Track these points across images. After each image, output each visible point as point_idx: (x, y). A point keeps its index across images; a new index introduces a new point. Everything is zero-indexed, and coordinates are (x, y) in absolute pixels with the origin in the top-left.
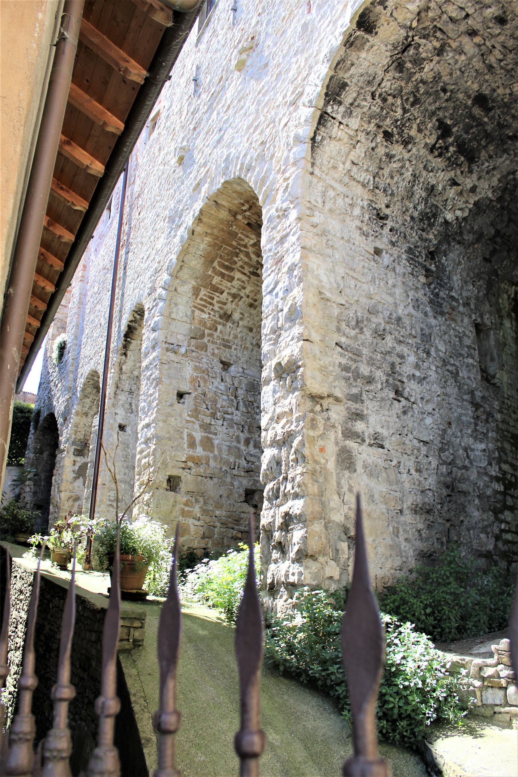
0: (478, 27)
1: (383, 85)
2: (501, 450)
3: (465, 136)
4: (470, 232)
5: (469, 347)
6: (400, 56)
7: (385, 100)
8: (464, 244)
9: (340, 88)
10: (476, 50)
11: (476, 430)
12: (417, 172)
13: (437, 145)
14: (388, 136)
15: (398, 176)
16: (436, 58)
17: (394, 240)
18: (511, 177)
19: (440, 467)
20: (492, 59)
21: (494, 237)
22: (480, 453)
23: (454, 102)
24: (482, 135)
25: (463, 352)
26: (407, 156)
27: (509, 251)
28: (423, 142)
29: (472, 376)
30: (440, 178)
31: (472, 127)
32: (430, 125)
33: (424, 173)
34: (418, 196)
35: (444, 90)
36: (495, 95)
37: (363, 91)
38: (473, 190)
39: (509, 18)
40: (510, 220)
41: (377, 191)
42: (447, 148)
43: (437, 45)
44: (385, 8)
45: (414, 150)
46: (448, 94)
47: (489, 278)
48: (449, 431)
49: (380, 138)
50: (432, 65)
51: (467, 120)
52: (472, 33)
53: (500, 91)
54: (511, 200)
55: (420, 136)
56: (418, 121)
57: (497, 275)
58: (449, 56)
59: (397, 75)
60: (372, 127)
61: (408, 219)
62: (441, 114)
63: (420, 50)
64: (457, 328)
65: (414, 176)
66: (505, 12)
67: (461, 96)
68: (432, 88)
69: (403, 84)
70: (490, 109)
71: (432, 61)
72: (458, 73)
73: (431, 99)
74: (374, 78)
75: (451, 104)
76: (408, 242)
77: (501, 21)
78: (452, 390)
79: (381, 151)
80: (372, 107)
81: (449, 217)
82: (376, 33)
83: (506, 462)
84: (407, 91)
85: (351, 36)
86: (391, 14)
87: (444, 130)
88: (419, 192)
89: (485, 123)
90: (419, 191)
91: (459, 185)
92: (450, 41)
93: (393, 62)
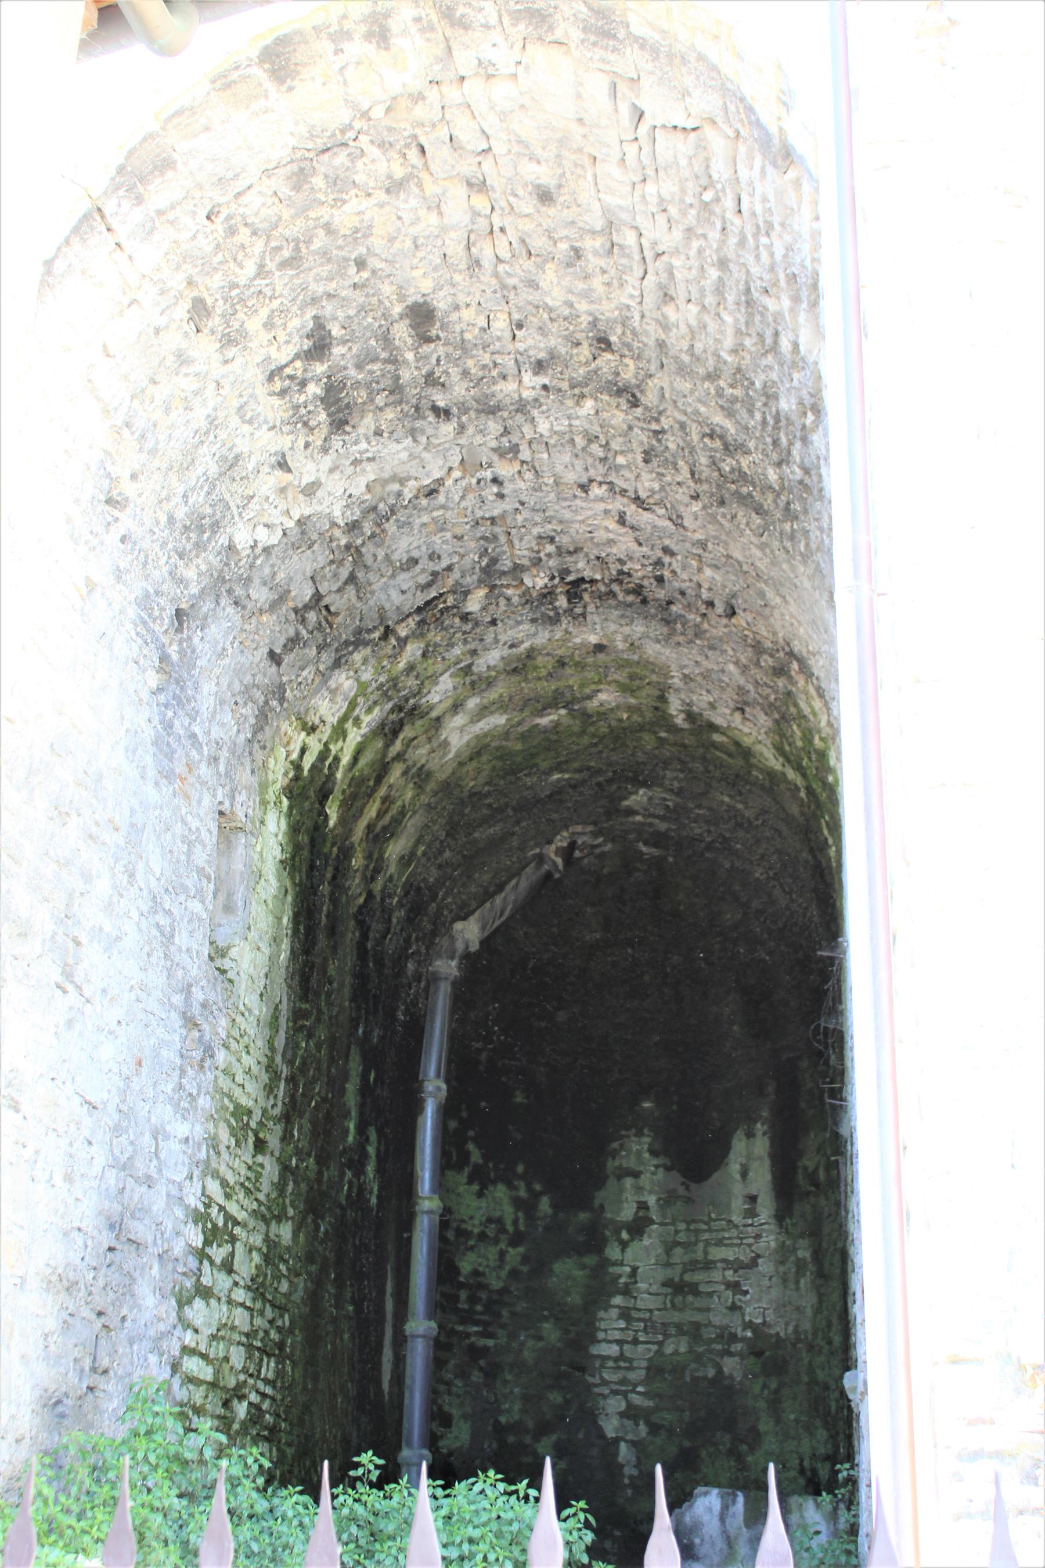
0: (496, 184)
1: (244, 199)
2: (213, 1143)
3: (352, 372)
4: (265, 584)
5: (201, 871)
6: (311, 155)
7: (232, 231)
8: (244, 607)
9: (155, 167)
10: (467, 219)
11: (180, 1087)
12: (221, 415)
13: (288, 371)
14: (200, 309)
15: (181, 410)
16: (382, 196)
17: (122, 565)
18: (395, 487)
19: (108, 1174)
20: (485, 251)
21: (307, 607)
22: (178, 1147)
23: (367, 295)
24: (387, 382)
25: (189, 883)
26: (217, 371)
27: (320, 649)
28: (263, 351)
29: (195, 946)
30: (260, 443)
31: (375, 360)
32: (296, 322)
33: (235, 421)
34: (200, 471)
35: (361, 264)
36: (454, 317)
37: (198, 194)
38: (310, 490)
39: (562, 199)
40: (352, 579)
41: (126, 432)
42: (303, 384)
43: (399, 172)
44: (338, 52)
45: (238, 361)
46: (365, 275)
47: (266, 703)
48: (136, 1085)
49: (182, 310)
50: (366, 203)
51: (373, 342)
52: (478, 186)
53: (467, 314)
54: (373, 536)
55: (265, 336)
56: (275, 304)
57: (282, 699)
58: (409, 203)
59: (285, 191)
60: (177, 282)
61: (164, 519)
62: (328, 308)
63: (359, 164)
64: (189, 818)
65: (212, 421)
66: (560, 186)
67: (387, 289)
68: (340, 248)
69: (286, 215)
70: (429, 340)
71: (369, 195)
72: (408, 243)
73: (325, 270)
74: (237, 176)
75: (359, 297)
76: (147, 577)
77: (545, 197)
78: (157, 979)
79: (173, 340)
80: (200, 236)
81: (242, 538)
82: (290, 89)
83: (216, 1175)
84: (287, 233)
85: (237, 68)
86: (342, 68)
87: (319, 345)
88: (208, 464)
89: (405, 362)
90: (208, 458)
91: (289, 471)
92: (424, 176)
93: (292, 161)
